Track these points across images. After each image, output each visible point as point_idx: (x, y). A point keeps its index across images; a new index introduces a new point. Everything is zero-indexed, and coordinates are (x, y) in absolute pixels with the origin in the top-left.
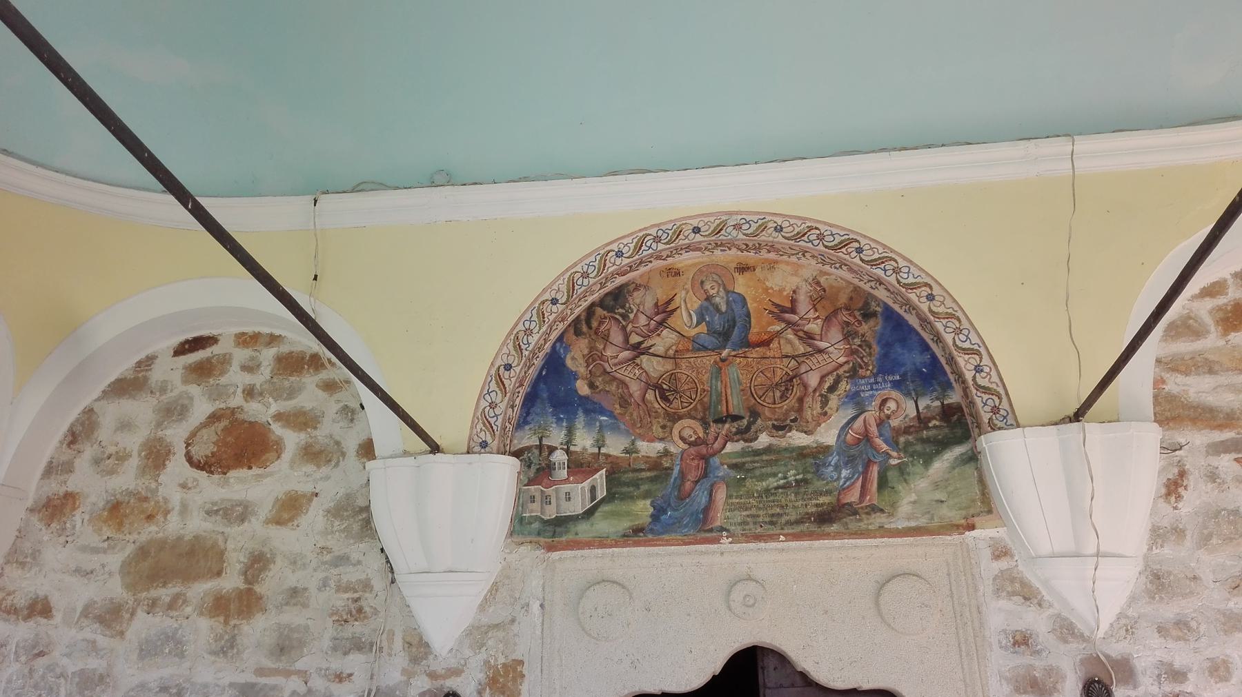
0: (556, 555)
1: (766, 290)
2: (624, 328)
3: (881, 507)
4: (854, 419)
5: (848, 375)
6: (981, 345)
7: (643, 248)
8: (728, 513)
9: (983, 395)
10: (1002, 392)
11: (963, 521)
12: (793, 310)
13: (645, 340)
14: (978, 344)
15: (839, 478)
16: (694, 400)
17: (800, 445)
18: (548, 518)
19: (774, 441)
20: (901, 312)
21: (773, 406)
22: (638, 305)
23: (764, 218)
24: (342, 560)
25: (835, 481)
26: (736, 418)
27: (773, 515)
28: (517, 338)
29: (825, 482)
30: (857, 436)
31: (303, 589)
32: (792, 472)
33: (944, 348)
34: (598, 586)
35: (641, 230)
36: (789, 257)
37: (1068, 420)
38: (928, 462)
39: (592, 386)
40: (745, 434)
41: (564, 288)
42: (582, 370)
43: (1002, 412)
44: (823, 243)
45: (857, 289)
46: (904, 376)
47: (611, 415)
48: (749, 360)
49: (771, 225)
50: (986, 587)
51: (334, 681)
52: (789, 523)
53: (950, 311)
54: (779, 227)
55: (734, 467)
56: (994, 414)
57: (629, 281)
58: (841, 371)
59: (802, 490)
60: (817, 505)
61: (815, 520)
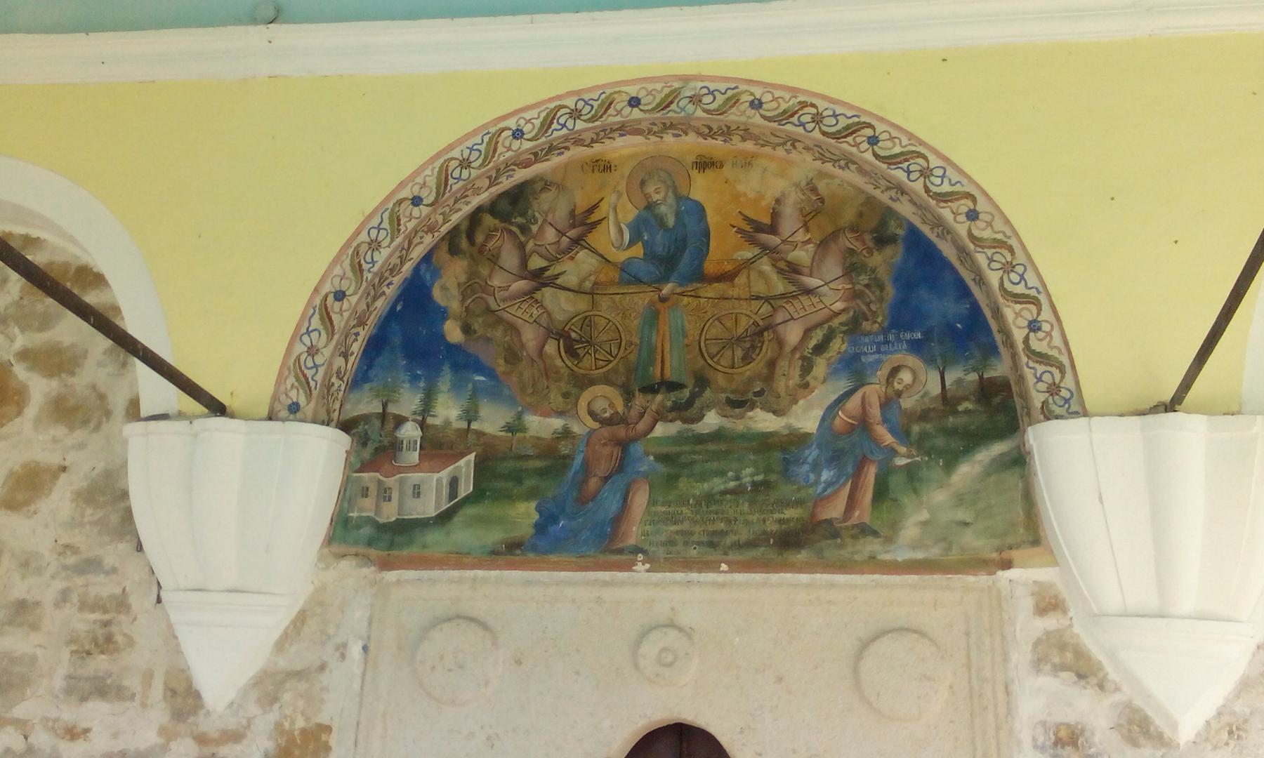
0: (392, 576)
1: (736, 196)
2: (522, 246)
3: (876, 528)
4: (848, 395)
5: (845, 328)
6: (1041, 289)
7: (553, 126)
8: (648, 527)
9: (1037, 366)
10: (1064, 359)
11: (995, 555)
12: (773, 229)
13: (550, 266)
14: (1036, 289)
15: (817, 482)
16: (615, 358)
17: (764, 431)
18: (385, 521)
19: (727, 423)
20: (932, 236)
21: (730, 371)
22: (546, 213)
23: (736, 88)
24: (91, 565)
25: (811, 486)
26: (673, 386)
27: (714, 533)
28: (358, 253)
29: (796, 487)
30: (850, 421)
31: (33, 603)
32: (749, 471)
33: (989, 293)
34: (446, 625)
35: (551, 100)
36: (774, 149)
37: (1162, 408)
38: (950, 466)
39: (467, 329)
40: (685, 410)
41: (432, 182)
42: (455, 306)
43: (1064, 393)
44: (820, 128)
45: (870, 201)
46: (928, 334)
47: (491, 374)
48: (702, 301)
49: (746, 98)
50: (1021, 656)
51: (63, 738)
52: (738, 546)
53: (999, 236)
54: (756, 102)
55: (664, 458)
56: (1052, 395)
57: (536, 176)
58: (835, 322)
59: (761, 497)
60: (781, 521)
61: (775, 542)
